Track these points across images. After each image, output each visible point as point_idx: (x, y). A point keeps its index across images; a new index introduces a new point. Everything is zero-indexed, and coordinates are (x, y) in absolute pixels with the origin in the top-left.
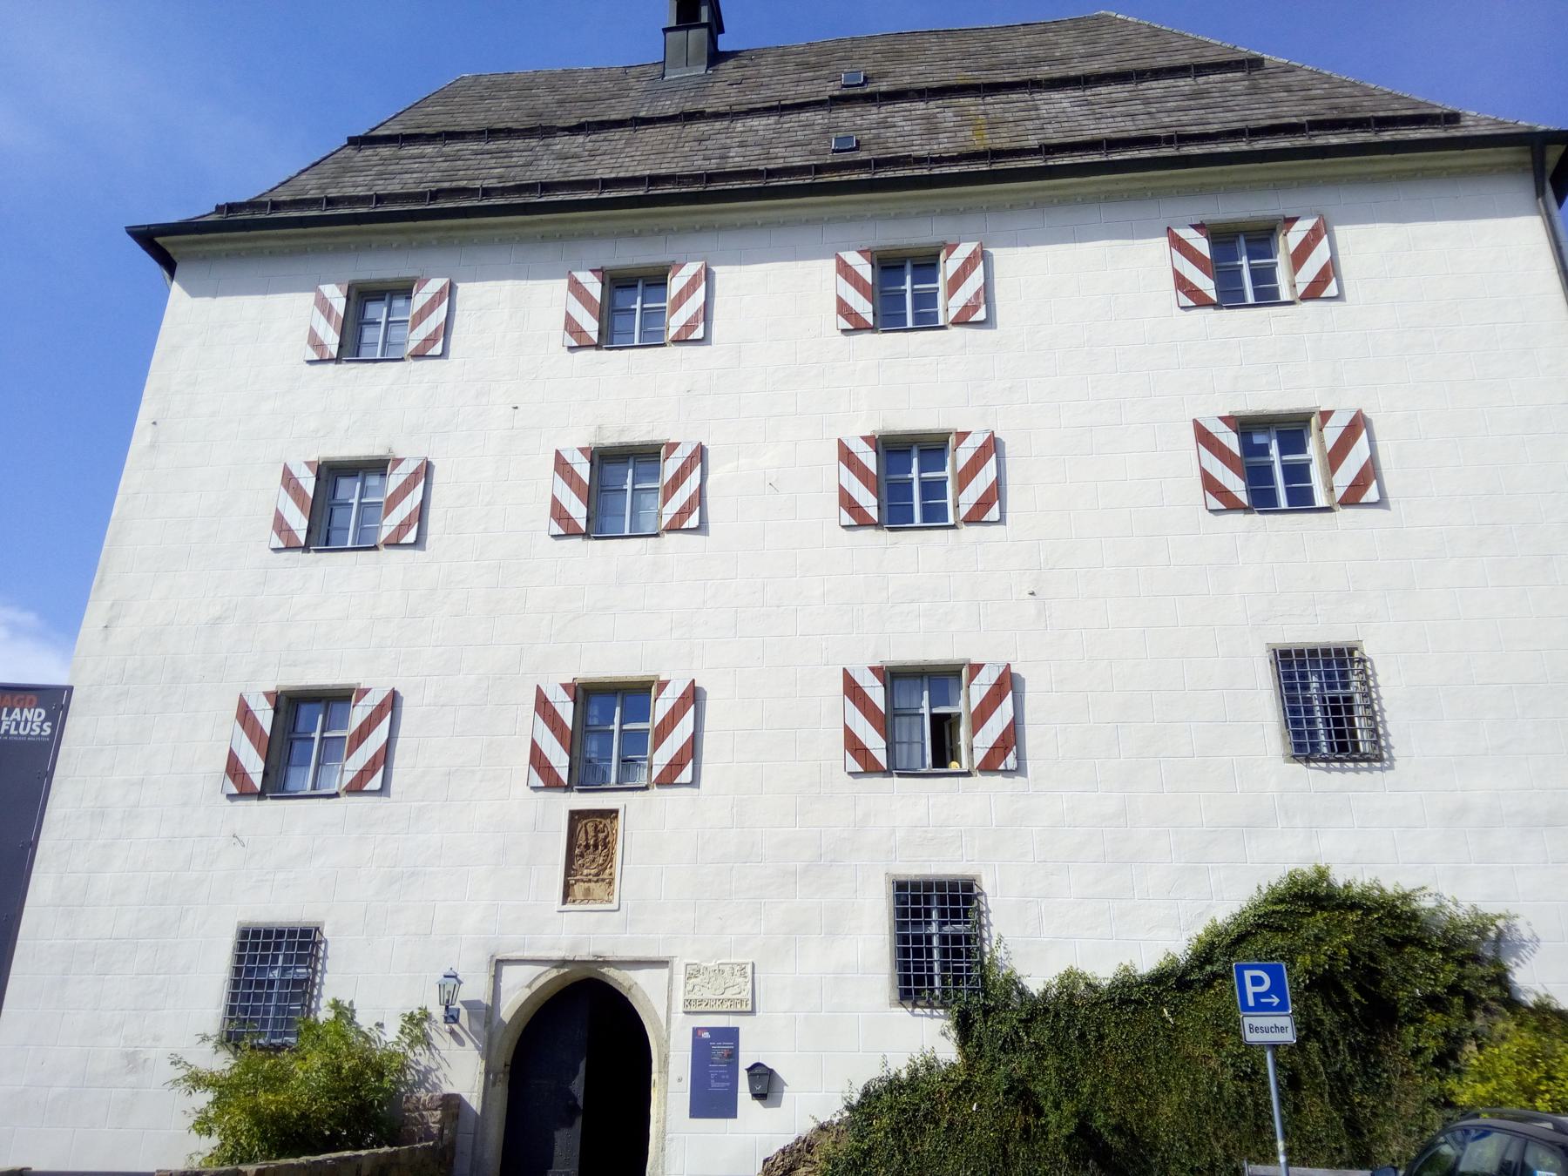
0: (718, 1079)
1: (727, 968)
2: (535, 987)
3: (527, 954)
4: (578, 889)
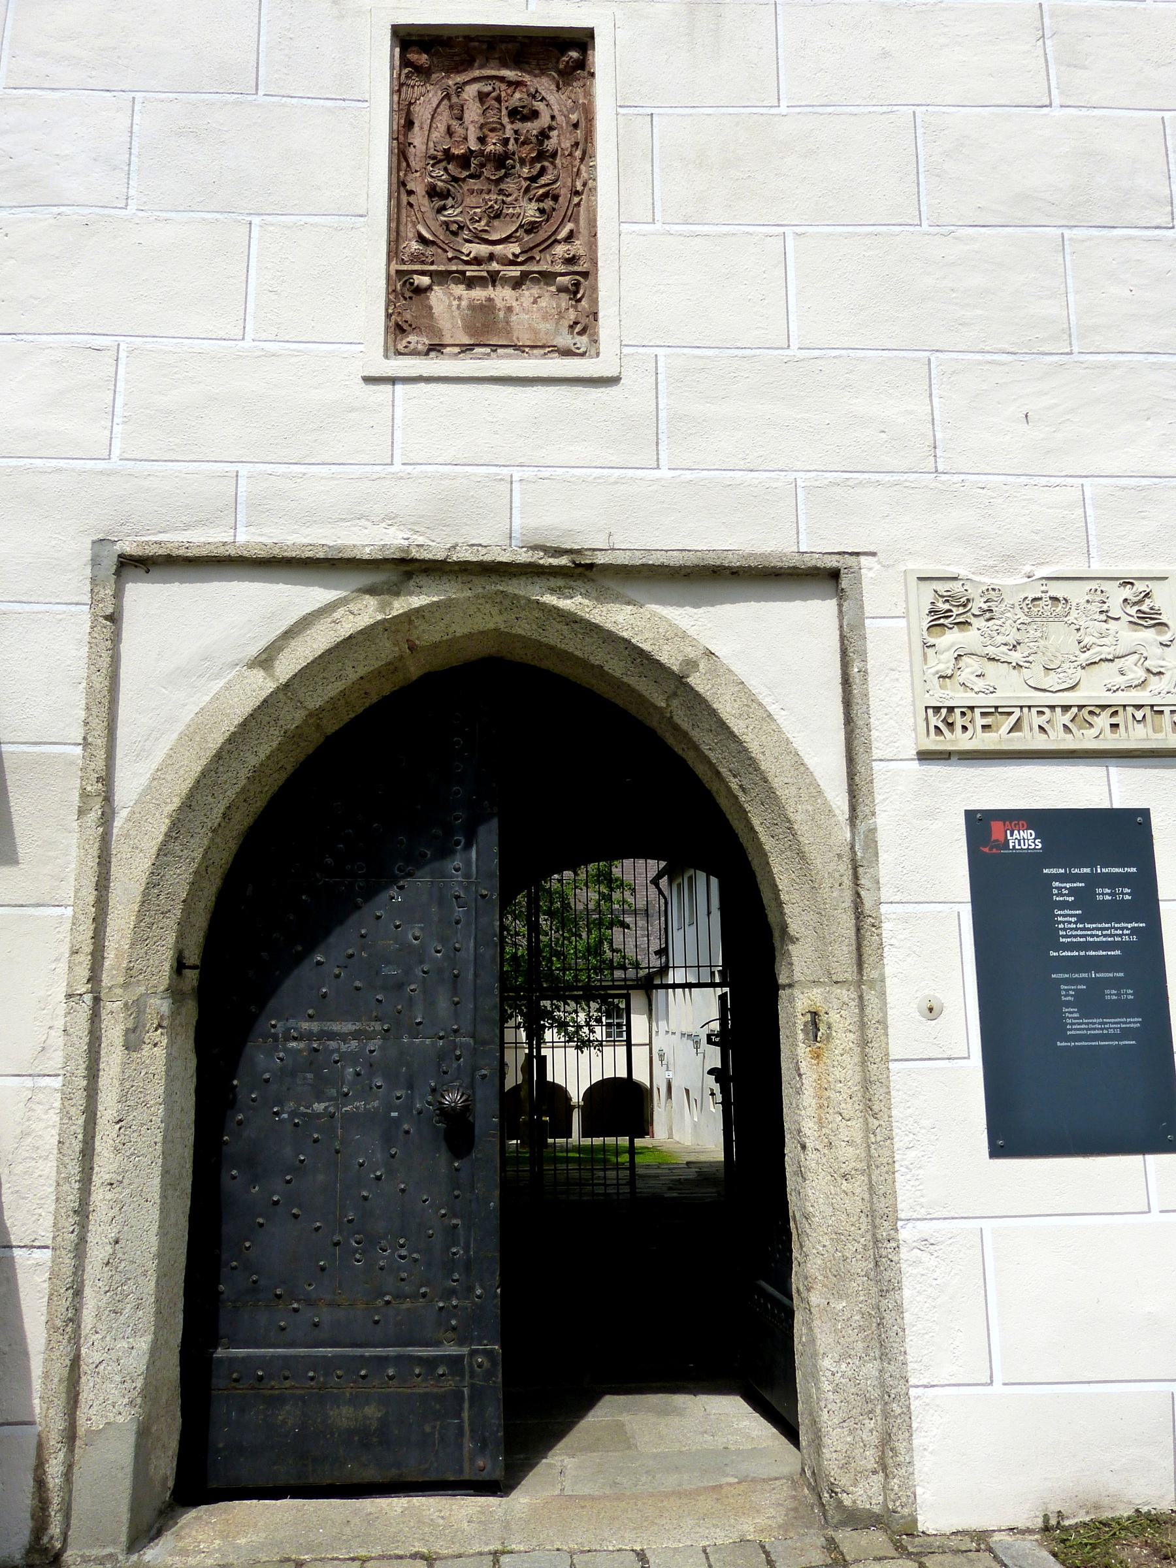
0: (1091, 1004)
1: (1076, 593)
2: (288, 665)
3: (248, 537)
4: (447, 304)
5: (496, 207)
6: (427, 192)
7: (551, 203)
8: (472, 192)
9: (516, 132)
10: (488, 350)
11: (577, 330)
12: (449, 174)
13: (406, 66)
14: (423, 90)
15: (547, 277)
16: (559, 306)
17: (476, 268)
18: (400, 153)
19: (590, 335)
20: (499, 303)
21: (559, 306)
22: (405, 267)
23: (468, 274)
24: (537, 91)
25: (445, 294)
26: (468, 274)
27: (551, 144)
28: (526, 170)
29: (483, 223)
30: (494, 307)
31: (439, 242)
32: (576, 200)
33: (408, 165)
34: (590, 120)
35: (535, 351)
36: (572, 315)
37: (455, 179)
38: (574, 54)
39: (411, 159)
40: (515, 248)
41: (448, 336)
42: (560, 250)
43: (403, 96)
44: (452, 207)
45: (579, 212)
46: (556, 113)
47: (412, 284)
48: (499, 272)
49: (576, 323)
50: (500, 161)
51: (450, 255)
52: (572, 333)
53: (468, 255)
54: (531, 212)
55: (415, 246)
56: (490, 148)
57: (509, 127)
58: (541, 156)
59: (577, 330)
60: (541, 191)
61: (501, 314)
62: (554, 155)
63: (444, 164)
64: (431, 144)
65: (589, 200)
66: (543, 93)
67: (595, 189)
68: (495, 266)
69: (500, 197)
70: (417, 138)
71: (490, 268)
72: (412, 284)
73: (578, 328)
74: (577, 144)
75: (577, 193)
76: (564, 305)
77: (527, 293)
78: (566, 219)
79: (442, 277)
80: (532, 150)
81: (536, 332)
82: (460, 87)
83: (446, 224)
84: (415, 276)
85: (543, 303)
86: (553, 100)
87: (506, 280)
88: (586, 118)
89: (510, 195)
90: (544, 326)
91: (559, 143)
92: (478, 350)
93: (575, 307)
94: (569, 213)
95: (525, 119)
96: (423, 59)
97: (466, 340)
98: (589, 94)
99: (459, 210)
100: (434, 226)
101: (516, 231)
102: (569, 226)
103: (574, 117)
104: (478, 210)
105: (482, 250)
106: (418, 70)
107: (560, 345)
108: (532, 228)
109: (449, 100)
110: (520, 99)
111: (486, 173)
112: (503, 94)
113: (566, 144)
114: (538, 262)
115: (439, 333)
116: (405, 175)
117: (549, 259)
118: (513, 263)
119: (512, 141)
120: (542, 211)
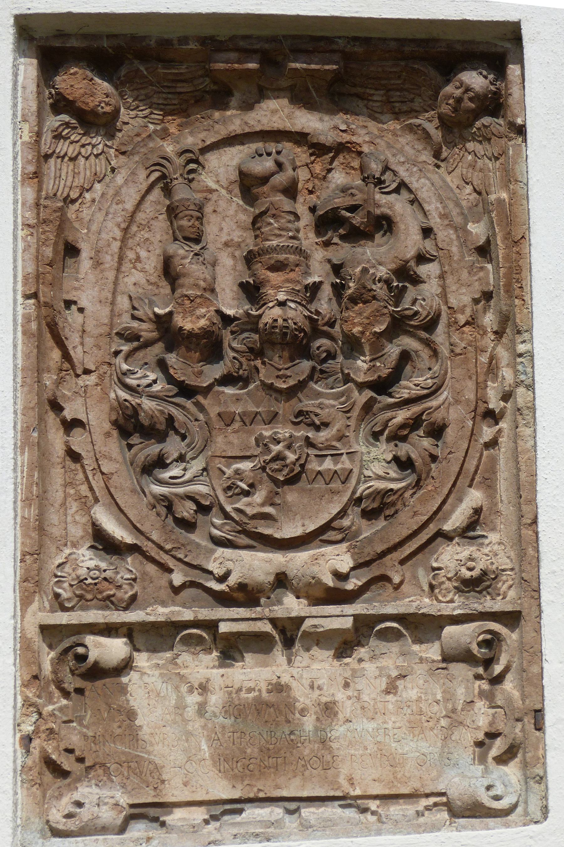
4: (172, 702)
5: (291, 457)
6: (115, 423)
7: (427, 443)
8: (227, 419)
9: (337, 269)
10: (276, 812)
11: (494, 752)
12: (171, 380)
13: (56, 109)
14: (100, 166)
15: (422, 626)
16: (449, 696)
17: (242, 612)
18: (47, 326)
19: (525, 765)
20: (302, 696)
21: (449, 696)
22: (63, 618)
23: (223, 628)
24: (386, 168)
25: (166, 678)
26: (223, 628)
27: (426, 296)
28: (362, 363)
29: (258, 497)
30: (290, 705)
31: (147, 546)
32: (487, 432)
33: (66, 356)
34: (518, 242)
35: (395, 810)
36: (482, 717)
37: (186, 391)
38: (475, 80)
39: (73, 341)
40: (340, 558)
41: (177, 781)
42: (451, 557)
43: (49, 186)
44: (181, 458)
45: (494, 461)
46: (435, 221)
47: (82, 658)
48: (300, 620)
49: (492, 736)
50: (296, 343)
51: (178, 579)
52: (482, 760)
53: (222, 579)
54: (378, 468)
55: (88, 560)
56: (271, 314)
57: (318, 255)
58: (399, 325)
59: (494, 752)
60: (401, 416)
61: (309, 723)
62: (431, 325)
63: (158, 349)
64: (123, 303)
65: (516, 438)
66: (403, 173)
67: (533, 409)
68: (292, 605)
69: (300, 433)
70: (87, 287)
71: (279, 612)
72: (82, 658)
73: (497, 747)
74: (488, 296)
75: (492, 416)
76: (461, 693)
77: (370, 668)
78: (463, 481)
79: (158, 636)
80: (377, 315)
81: (394, 762)
82: (194, 159)
83: (168, 504)
84: (90, 639)
85: (410, 691)
86: (429, 186)
87: (319, 639)
88: (508, 235)
89: (326, 425)
90: (415, 748)
91: (444, 295)
92: (253, 813)
93: (489, 697)
94: (471, 465)
95: (356, 235)
96: (98, 91)
97: (223, 790)
98: (512, 178)
99: (196, 466)
100: (137, 509)
101: (342, 513)
102: (475, 497)
103: (478, 230)
104: (246, 466)
105: (255, 565)
106: (92, 121)
107: (453, 793)
108: (379, 506)
109: (167, 191)
110: (344, 190)
111: (265, 374)
112: (303, 175)
113: (462, 298)
114: (397, 587)
115: (152, 774)
116: (60, 382)
117: (424, 578)
118: (336, 597)
119: (327, 291)
120: (404, 464)
